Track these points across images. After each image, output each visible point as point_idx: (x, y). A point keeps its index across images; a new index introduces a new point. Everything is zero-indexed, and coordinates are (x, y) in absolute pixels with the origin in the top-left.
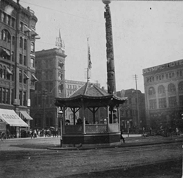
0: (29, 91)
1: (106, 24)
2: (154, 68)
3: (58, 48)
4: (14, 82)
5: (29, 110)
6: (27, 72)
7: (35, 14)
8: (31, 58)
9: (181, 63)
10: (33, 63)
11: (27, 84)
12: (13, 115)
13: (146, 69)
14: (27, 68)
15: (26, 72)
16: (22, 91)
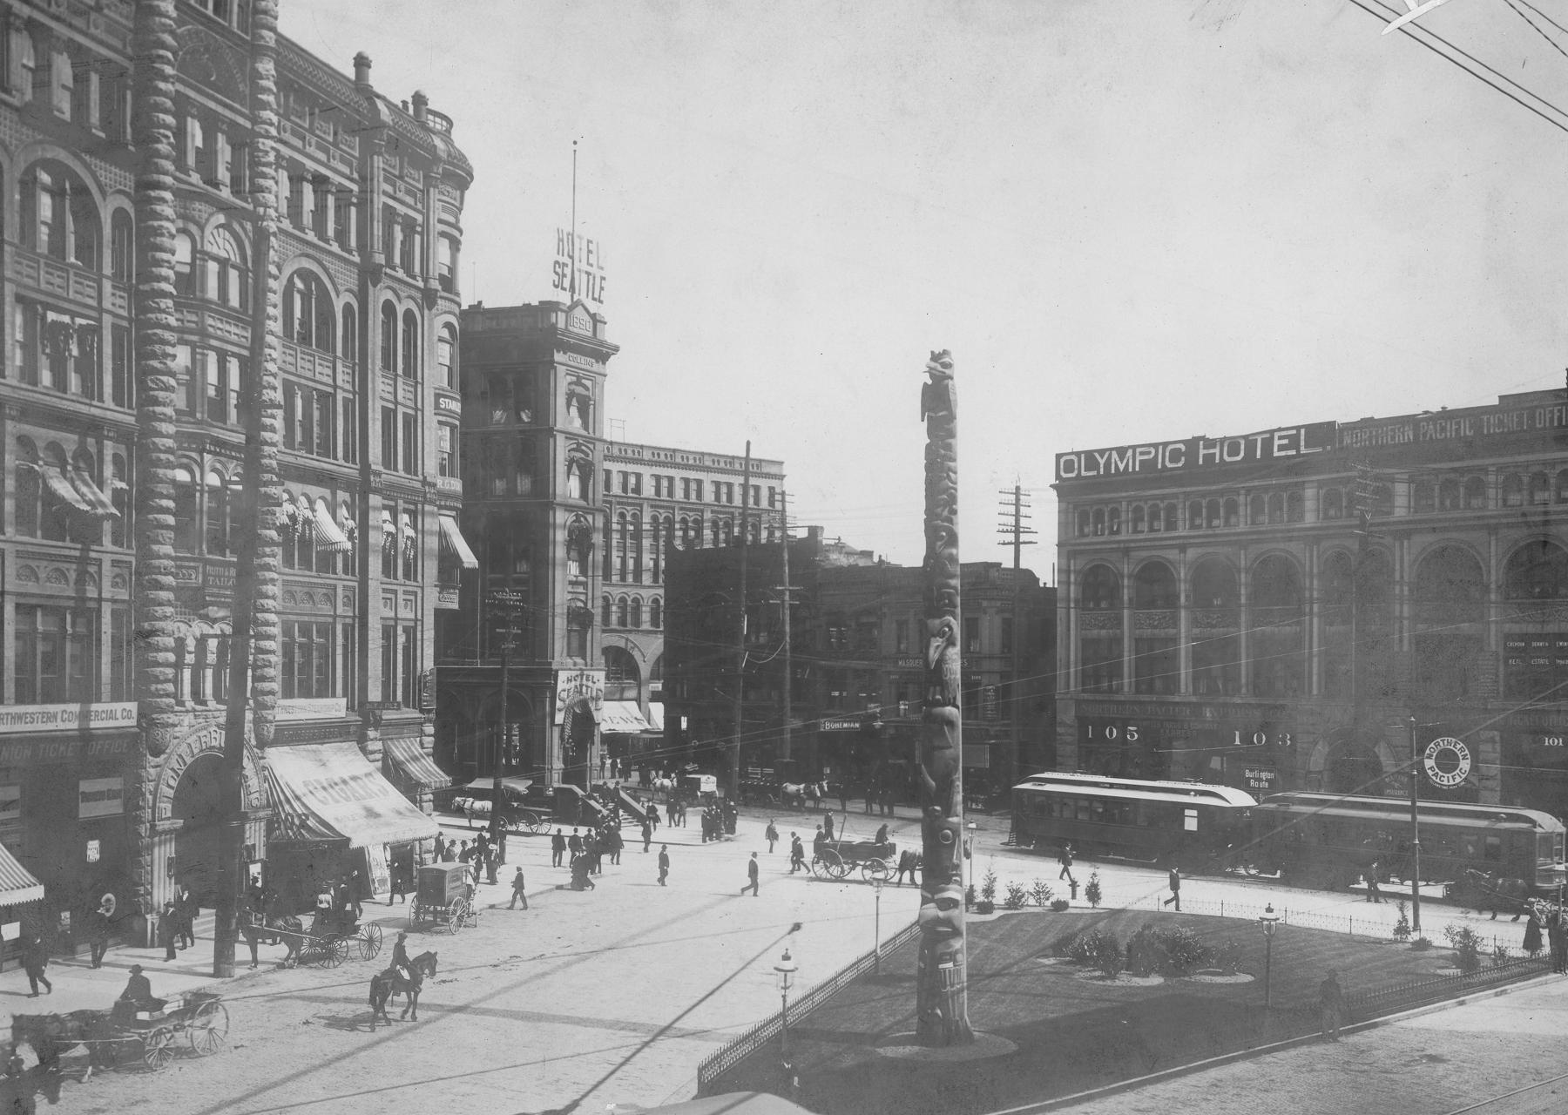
0: (429, 621)
2: (1122, 451)
3: (564, 298)
5: (430, 729)
9: (1281, 448)
13: (1078, 454)
14: (418, 485)
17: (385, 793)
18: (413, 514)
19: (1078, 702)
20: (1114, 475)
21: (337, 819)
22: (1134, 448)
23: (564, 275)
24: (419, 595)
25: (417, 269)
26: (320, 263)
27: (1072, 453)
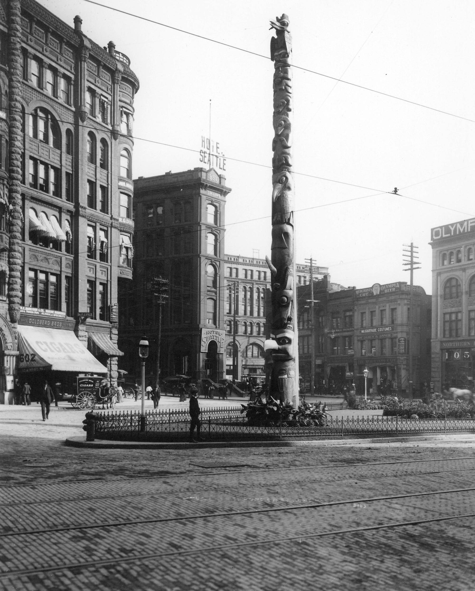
1: (276, 76)
2: (462, 223)
3: (206, 167)
4: (71, 257)
6: (109, 229)
7: (132, 67)
8: (121, 193)
10: (129, 205)
11: (109, 264)
12: (67, 344)
13: (441, 227)
15: (107, 231)
16: (95, 282)
17: (83, 352)
18: (106, 232)
19: (442, 342)
20: (459, 235)
21: (49, 358)
22: (467, 221)
23: (205, 157)
24: (109, 269)
25: (109, 121)
26: (52, 107)
27: (439, 227)
